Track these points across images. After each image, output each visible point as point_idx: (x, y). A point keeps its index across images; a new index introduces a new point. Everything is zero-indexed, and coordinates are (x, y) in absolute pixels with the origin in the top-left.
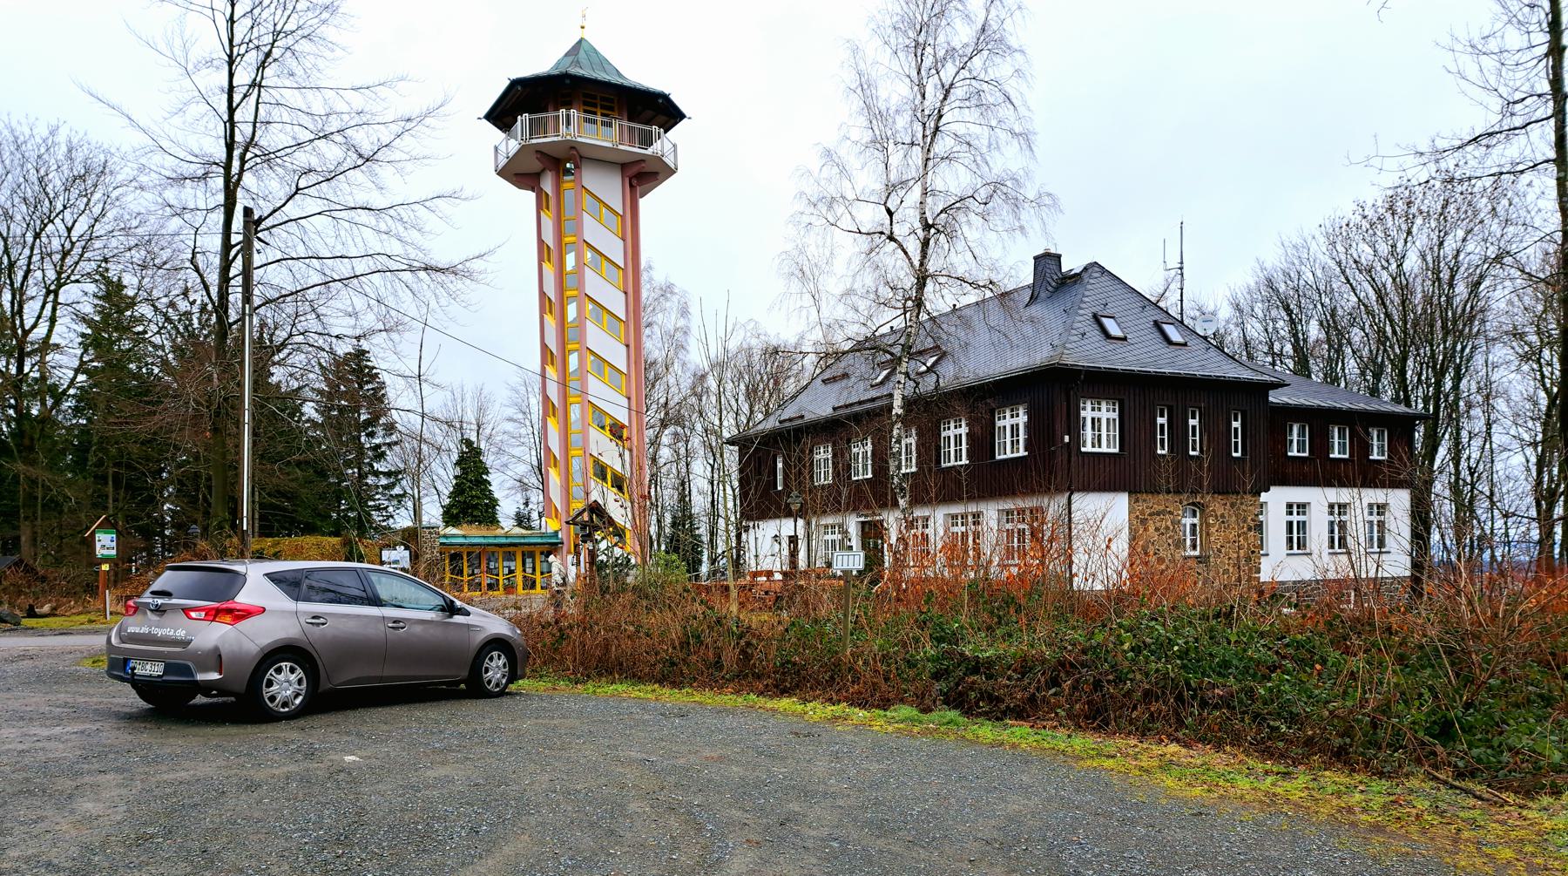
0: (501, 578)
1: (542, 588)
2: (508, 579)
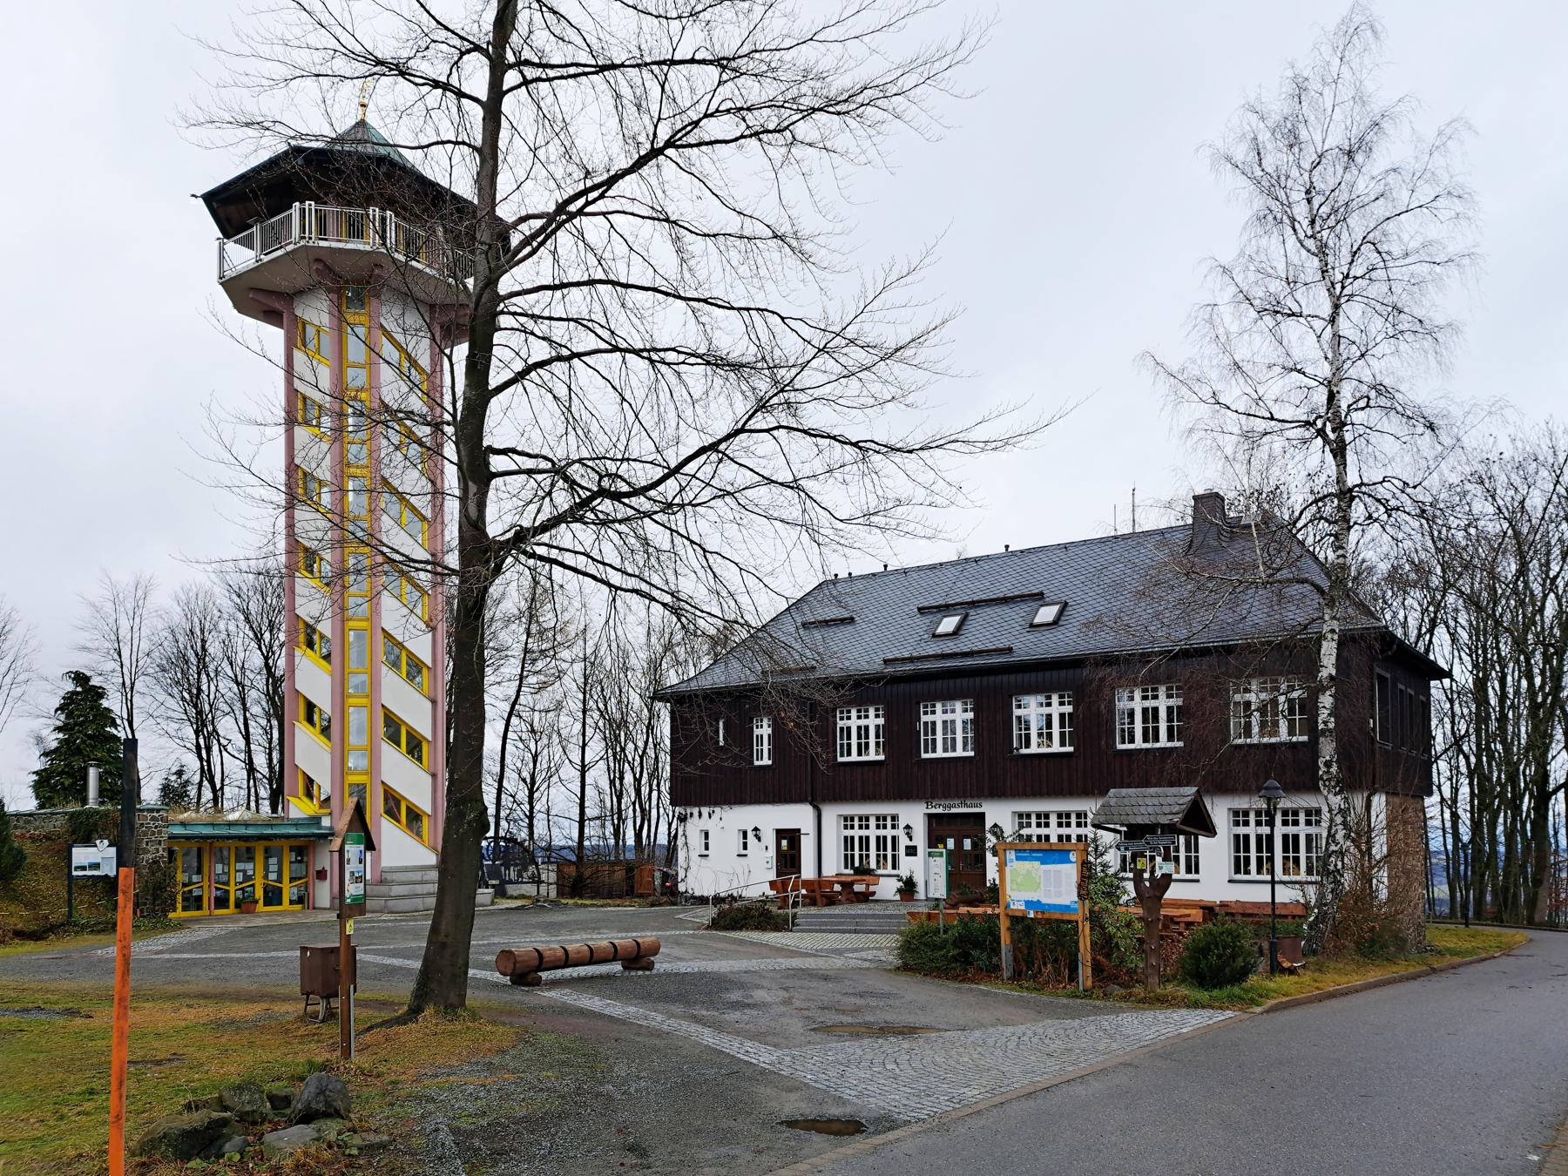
0: (232, 888)
1: (291, 902)
2: (242, 889)
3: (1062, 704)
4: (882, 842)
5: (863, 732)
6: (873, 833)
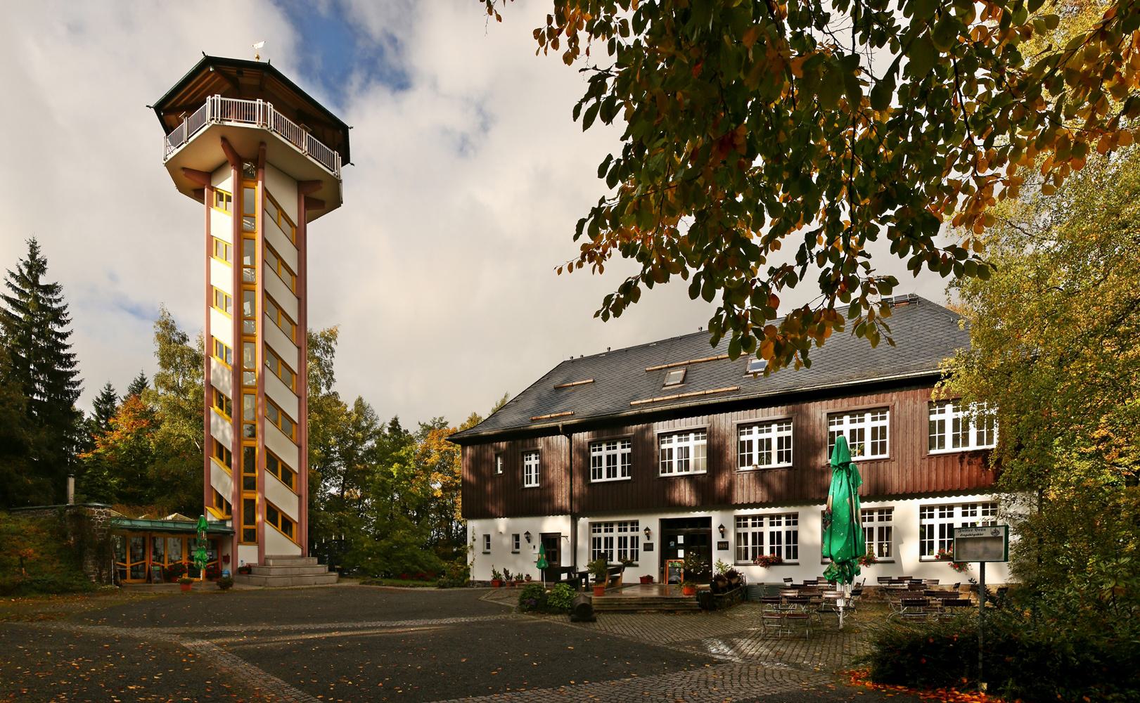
3: (623, 447)
4: (623, 541)
5: (612, 459)
6: (616, 534)
